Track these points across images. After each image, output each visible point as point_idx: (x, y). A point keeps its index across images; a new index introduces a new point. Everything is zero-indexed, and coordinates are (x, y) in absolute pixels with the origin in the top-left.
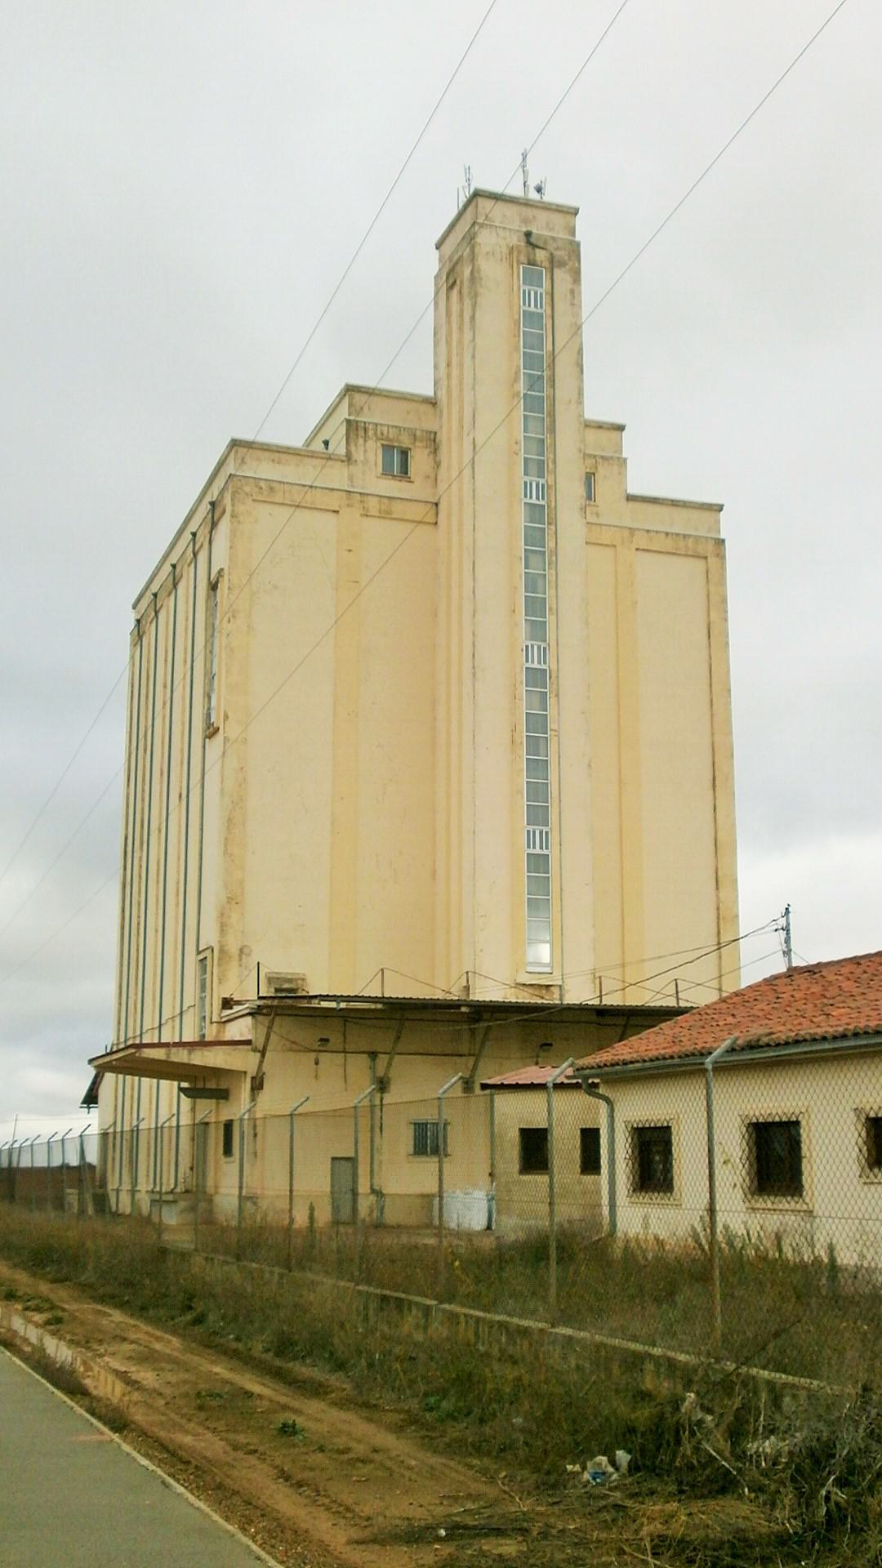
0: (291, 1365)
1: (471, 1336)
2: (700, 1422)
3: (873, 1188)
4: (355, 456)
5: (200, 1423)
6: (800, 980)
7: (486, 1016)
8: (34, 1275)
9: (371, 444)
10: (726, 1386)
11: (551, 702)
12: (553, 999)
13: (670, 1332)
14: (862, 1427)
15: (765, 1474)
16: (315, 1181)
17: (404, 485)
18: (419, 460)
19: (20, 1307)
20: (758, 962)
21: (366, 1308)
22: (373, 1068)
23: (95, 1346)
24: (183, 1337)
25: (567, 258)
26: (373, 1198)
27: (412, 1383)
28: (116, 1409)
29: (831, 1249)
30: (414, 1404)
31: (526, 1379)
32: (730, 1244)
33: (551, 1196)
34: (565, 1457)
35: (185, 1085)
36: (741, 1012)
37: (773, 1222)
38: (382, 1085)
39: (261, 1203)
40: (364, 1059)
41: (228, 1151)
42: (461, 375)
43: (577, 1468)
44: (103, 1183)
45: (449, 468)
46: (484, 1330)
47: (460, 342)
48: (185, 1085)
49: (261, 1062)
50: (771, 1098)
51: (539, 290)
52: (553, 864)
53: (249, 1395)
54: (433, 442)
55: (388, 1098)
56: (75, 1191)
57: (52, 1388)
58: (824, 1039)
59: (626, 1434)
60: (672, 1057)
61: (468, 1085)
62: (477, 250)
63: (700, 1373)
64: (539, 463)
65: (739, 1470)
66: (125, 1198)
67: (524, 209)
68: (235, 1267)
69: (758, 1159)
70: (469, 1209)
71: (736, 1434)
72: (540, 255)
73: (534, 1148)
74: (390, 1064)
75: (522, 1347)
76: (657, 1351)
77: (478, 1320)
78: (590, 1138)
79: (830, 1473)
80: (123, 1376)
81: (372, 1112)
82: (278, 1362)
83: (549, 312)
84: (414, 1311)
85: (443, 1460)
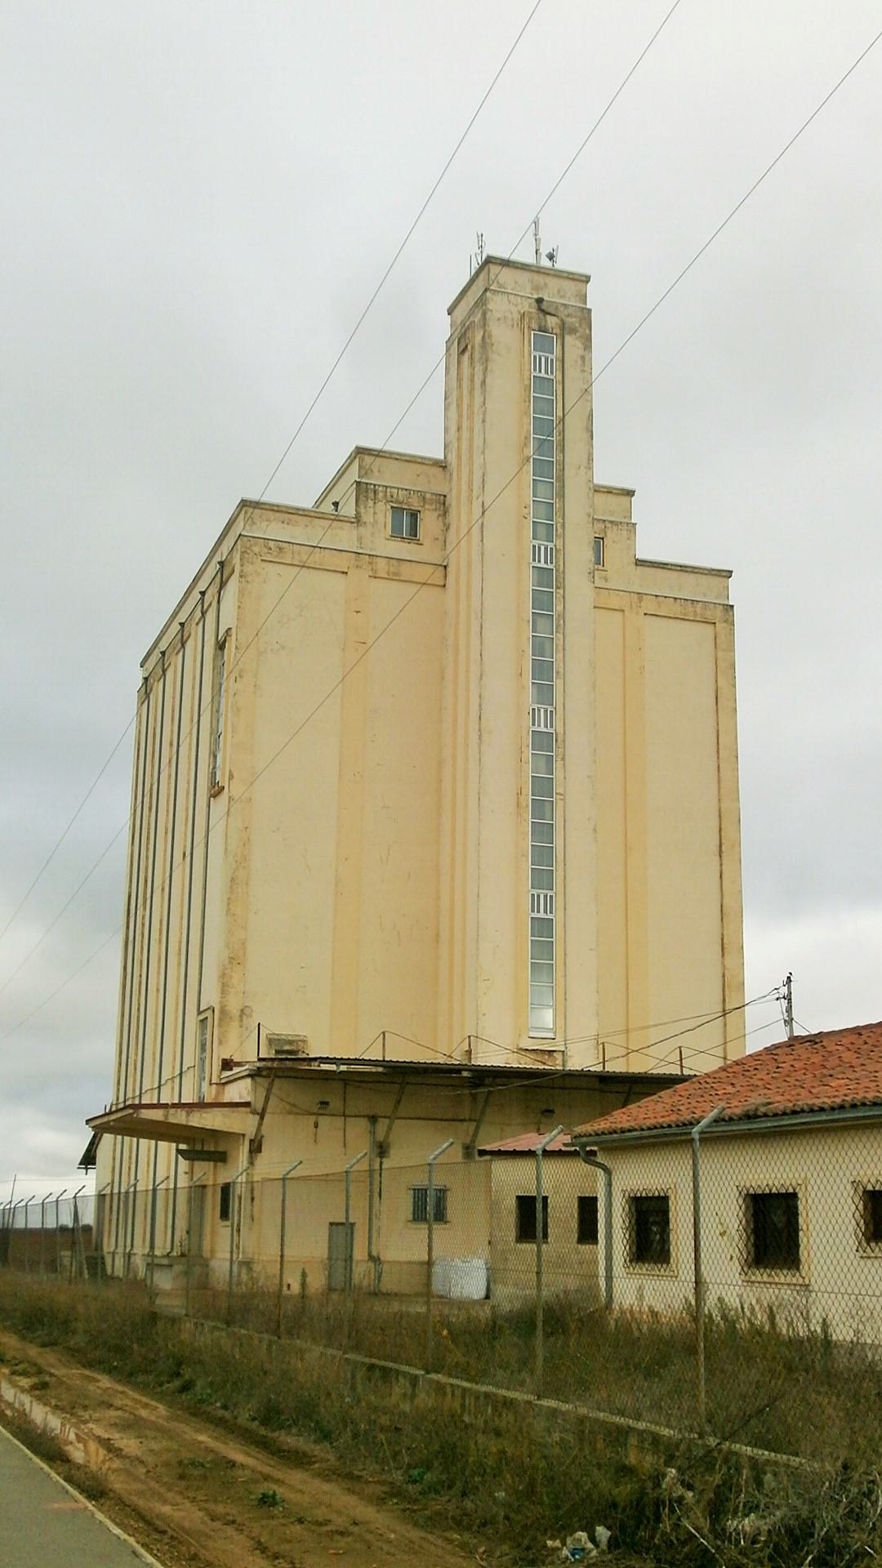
0: (276, 1434)
1: (457, 1405)
2: (680, 1500)
3: (869, 1262)
4: (365, 518)
5: (181, 1493)
6: (801, 1050)
7: (487, 1081)
8: (23, 1338)
9: (381, 506)
10: (708, 1461)
11: (558, 765)
12: (556, 1065)
13: (656, 1406)
14: (842, 1505)
15: (743, 1552)
16: (309, 1248)
17: (413, 547)
18: (429, 522)
19: (6, 1371)
20: (762, 1030)
21: (353, 1377)
22: (373, 1133)
23: (81, 1413)
24: (170, 1404)
25: (580, 324)
26: (371, 1264)
27: (396, 1455)
28: (94, 1477)
29: (825, 1325)
30: (398, 1476)
31: (510, 1451)
32: (724, 1317)
33: (539, 1266)
34: (545, 1533)
35: (183, 1147)
36: (740, 1081)
37: (769, 1294)
38: (382, 1150)
39: (257, 1268)
40: (364, 1123)
41: (225, 1214)
42: (471, 440)
43: (558, 1543)
44: (99, 1247)
45: (458, 531)
46: (470, 1401)
47: (471, 406)
48: (183, 1147)
49: (260, 1125)
50: (770, 1169)
51: (550, 356)
52: (558, 929)
53: (232, 1464)
54: (442, 504)
55: (387, 1163)
56: (68, 1253)
57: (31, 1455)
58: (822, 1110)
59: (606, 1511)
60: (670, 1126)
61: (468, 1151)
62: (489, 315)
63: (682, 1447)
64: (548, 525)
65: (718, 1548)
66: (119, 1262)
67: (536, 276)
68: (224, 1334)
69: (755, 1231)
70: (467, 1279)
71: (717, 1510)
72: (551, 321)
73: (530, 1216)
74: (390, 1128)
75: (507, 1420)
76: (641, 1425)
77: (464, 1390)
78: (587, 1206)
79: (808, 1553)
80: (107, 1444)
81: (371, 1177)
82: (263, 1431)
83: (559, 378)
84: (401, 1380)
85: (423, 1534)
